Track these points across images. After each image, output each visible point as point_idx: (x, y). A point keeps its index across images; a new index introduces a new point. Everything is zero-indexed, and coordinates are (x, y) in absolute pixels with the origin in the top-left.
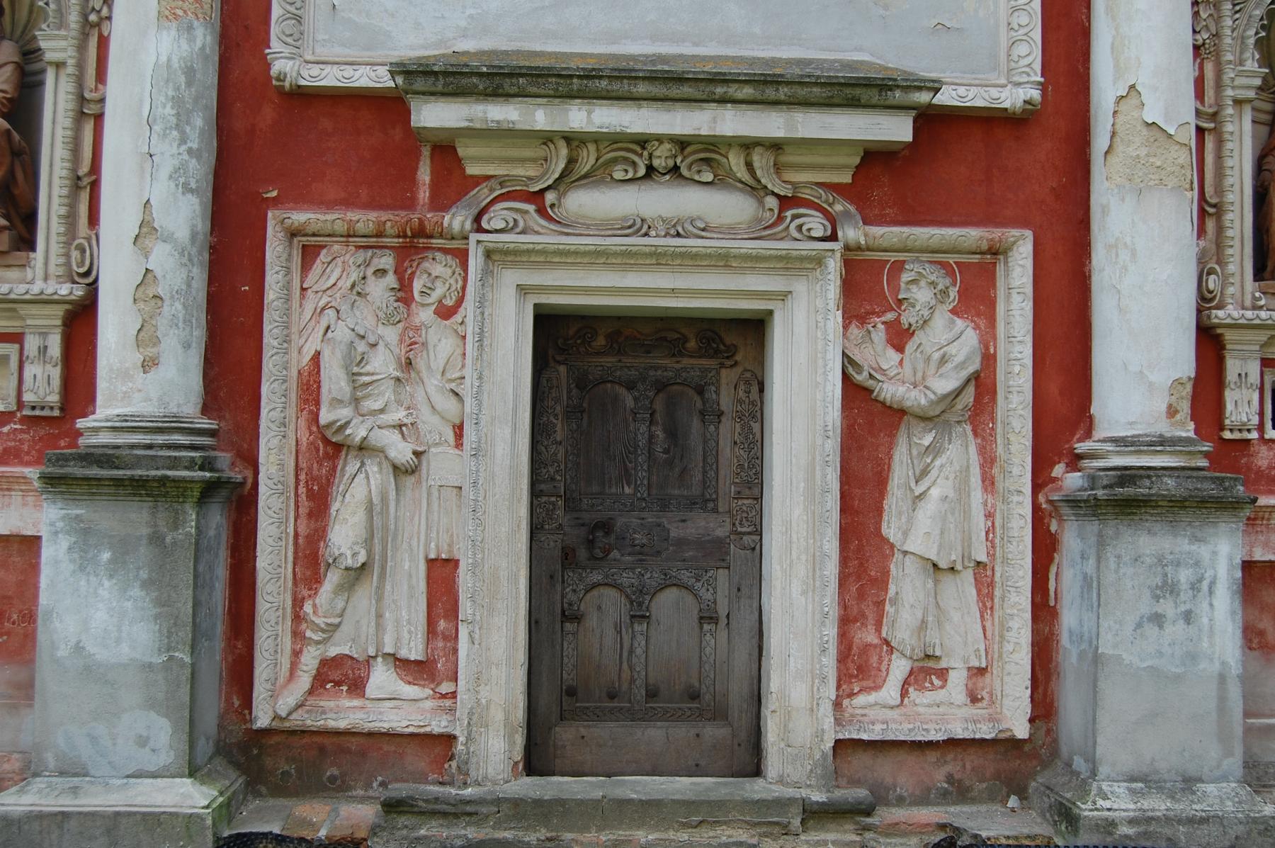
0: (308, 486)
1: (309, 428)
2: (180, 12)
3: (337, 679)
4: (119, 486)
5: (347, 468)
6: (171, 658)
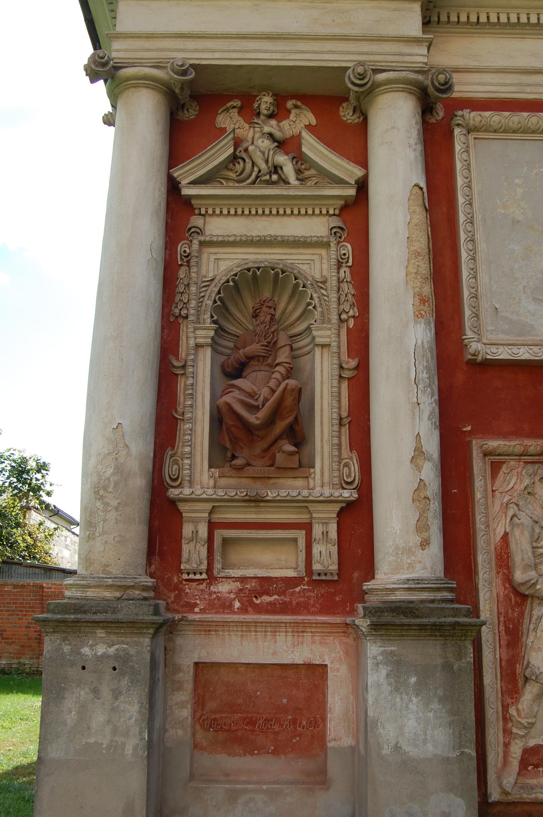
0: (506, 625)
1: (504, 585)
2: (423, 313)
3: (535, 763)
4: (422, 630)
5: (534, 612)
6: (462, 753)
